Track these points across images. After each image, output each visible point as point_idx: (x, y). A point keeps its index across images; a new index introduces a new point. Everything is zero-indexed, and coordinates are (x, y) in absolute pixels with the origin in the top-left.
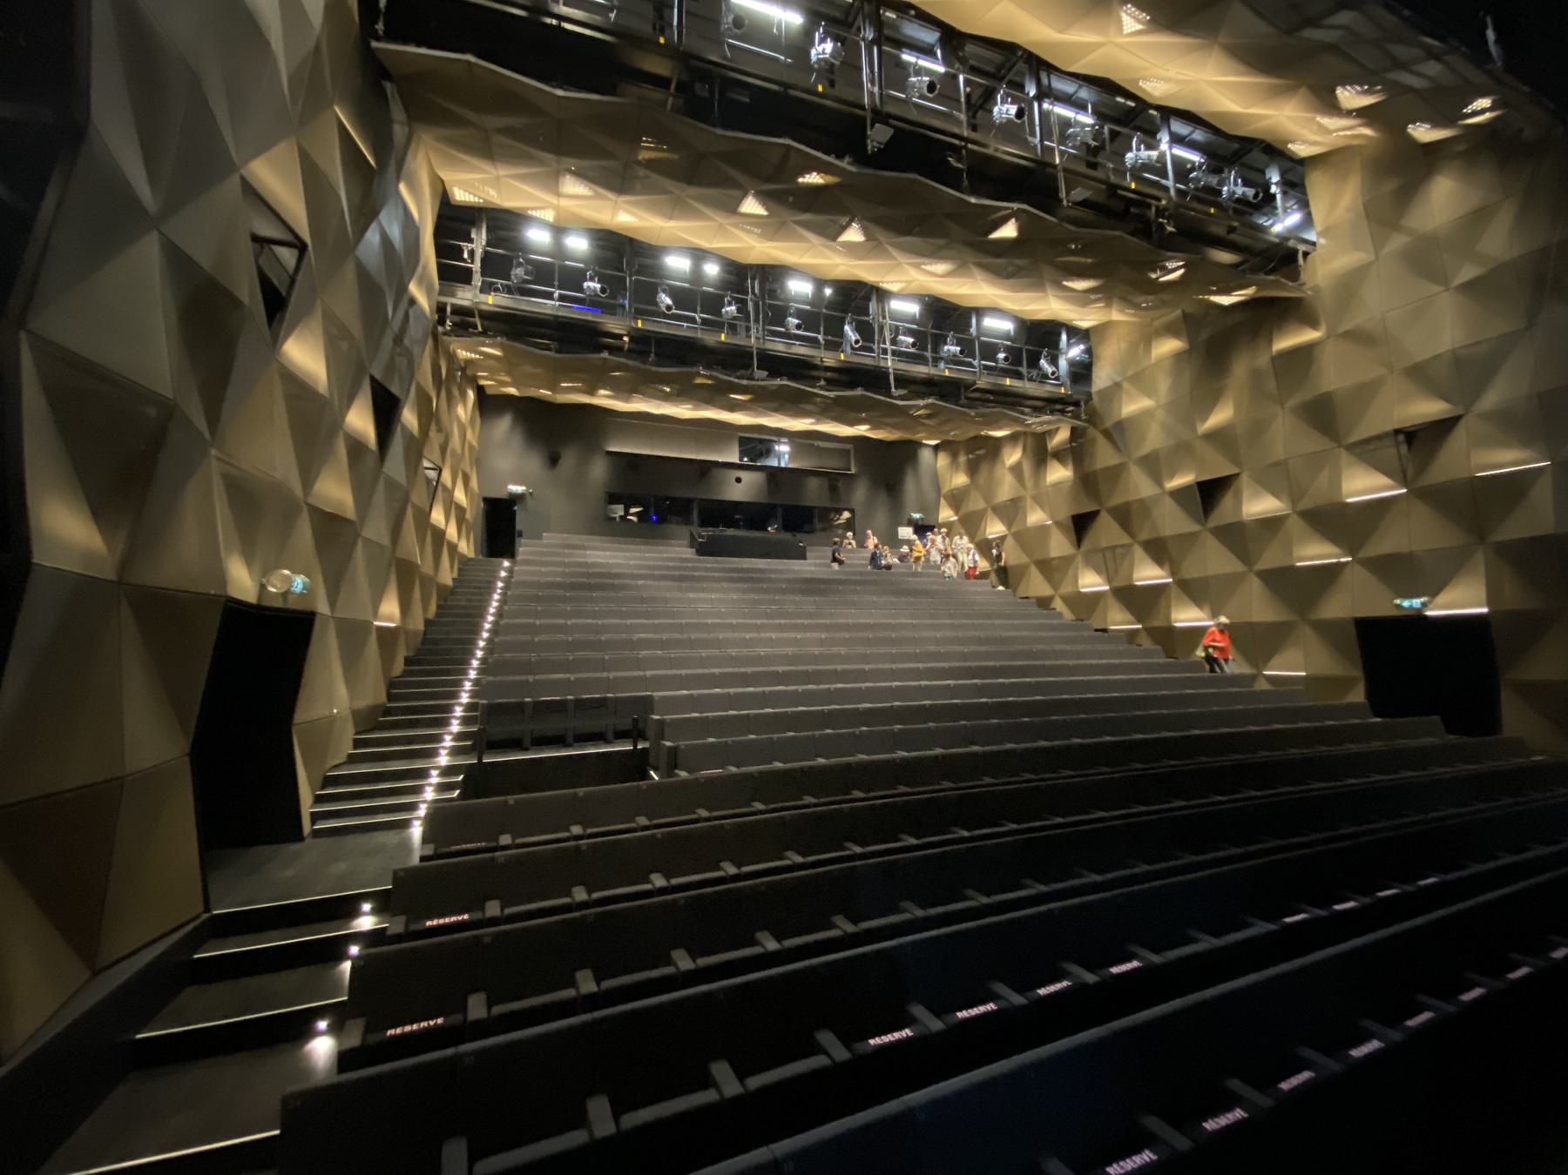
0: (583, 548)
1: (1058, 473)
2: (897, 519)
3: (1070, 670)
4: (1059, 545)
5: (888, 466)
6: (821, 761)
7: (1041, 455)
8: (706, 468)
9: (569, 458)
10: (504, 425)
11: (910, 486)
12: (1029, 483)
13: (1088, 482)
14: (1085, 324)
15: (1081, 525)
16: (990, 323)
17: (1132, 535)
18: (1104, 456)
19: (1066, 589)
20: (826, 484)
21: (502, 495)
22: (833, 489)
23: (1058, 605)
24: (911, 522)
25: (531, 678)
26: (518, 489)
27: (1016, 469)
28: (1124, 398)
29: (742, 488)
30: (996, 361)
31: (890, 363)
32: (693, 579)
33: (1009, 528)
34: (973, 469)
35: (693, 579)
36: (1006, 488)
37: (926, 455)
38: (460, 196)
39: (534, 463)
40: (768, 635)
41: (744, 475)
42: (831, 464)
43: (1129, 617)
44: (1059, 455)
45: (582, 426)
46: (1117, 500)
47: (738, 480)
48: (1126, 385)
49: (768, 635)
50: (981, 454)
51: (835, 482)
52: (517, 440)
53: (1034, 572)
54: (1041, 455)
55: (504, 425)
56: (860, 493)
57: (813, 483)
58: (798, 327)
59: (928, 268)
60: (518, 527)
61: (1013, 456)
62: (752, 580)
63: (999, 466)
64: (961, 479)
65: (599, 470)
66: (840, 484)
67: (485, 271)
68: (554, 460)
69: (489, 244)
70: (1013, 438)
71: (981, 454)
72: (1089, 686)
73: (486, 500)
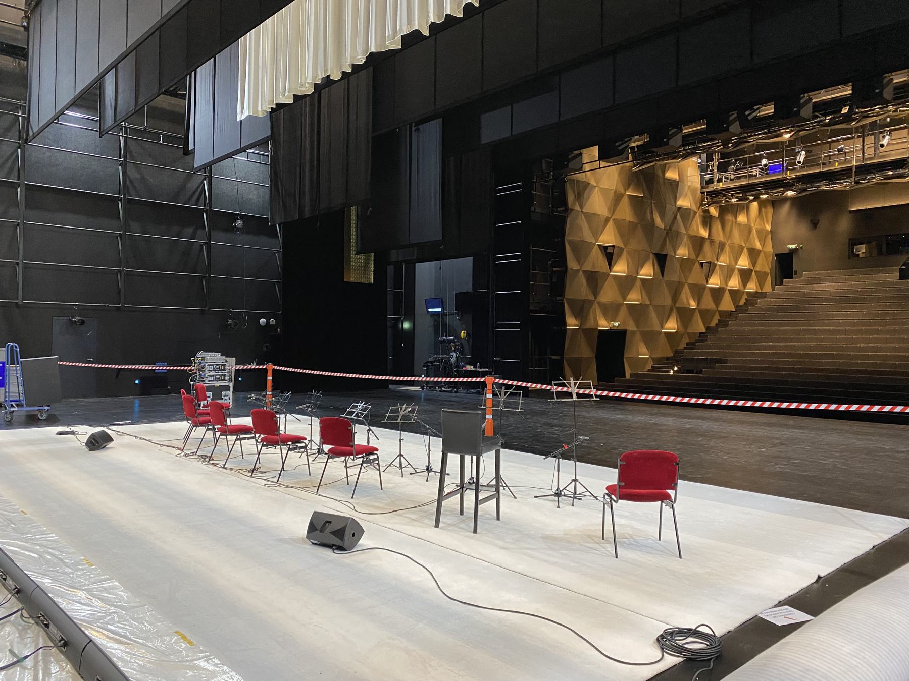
9: (824, 221)
21: (787, 251)
26: (794, 246)
52: (793, 218)
65: (844, 225)
68: (815, 225)
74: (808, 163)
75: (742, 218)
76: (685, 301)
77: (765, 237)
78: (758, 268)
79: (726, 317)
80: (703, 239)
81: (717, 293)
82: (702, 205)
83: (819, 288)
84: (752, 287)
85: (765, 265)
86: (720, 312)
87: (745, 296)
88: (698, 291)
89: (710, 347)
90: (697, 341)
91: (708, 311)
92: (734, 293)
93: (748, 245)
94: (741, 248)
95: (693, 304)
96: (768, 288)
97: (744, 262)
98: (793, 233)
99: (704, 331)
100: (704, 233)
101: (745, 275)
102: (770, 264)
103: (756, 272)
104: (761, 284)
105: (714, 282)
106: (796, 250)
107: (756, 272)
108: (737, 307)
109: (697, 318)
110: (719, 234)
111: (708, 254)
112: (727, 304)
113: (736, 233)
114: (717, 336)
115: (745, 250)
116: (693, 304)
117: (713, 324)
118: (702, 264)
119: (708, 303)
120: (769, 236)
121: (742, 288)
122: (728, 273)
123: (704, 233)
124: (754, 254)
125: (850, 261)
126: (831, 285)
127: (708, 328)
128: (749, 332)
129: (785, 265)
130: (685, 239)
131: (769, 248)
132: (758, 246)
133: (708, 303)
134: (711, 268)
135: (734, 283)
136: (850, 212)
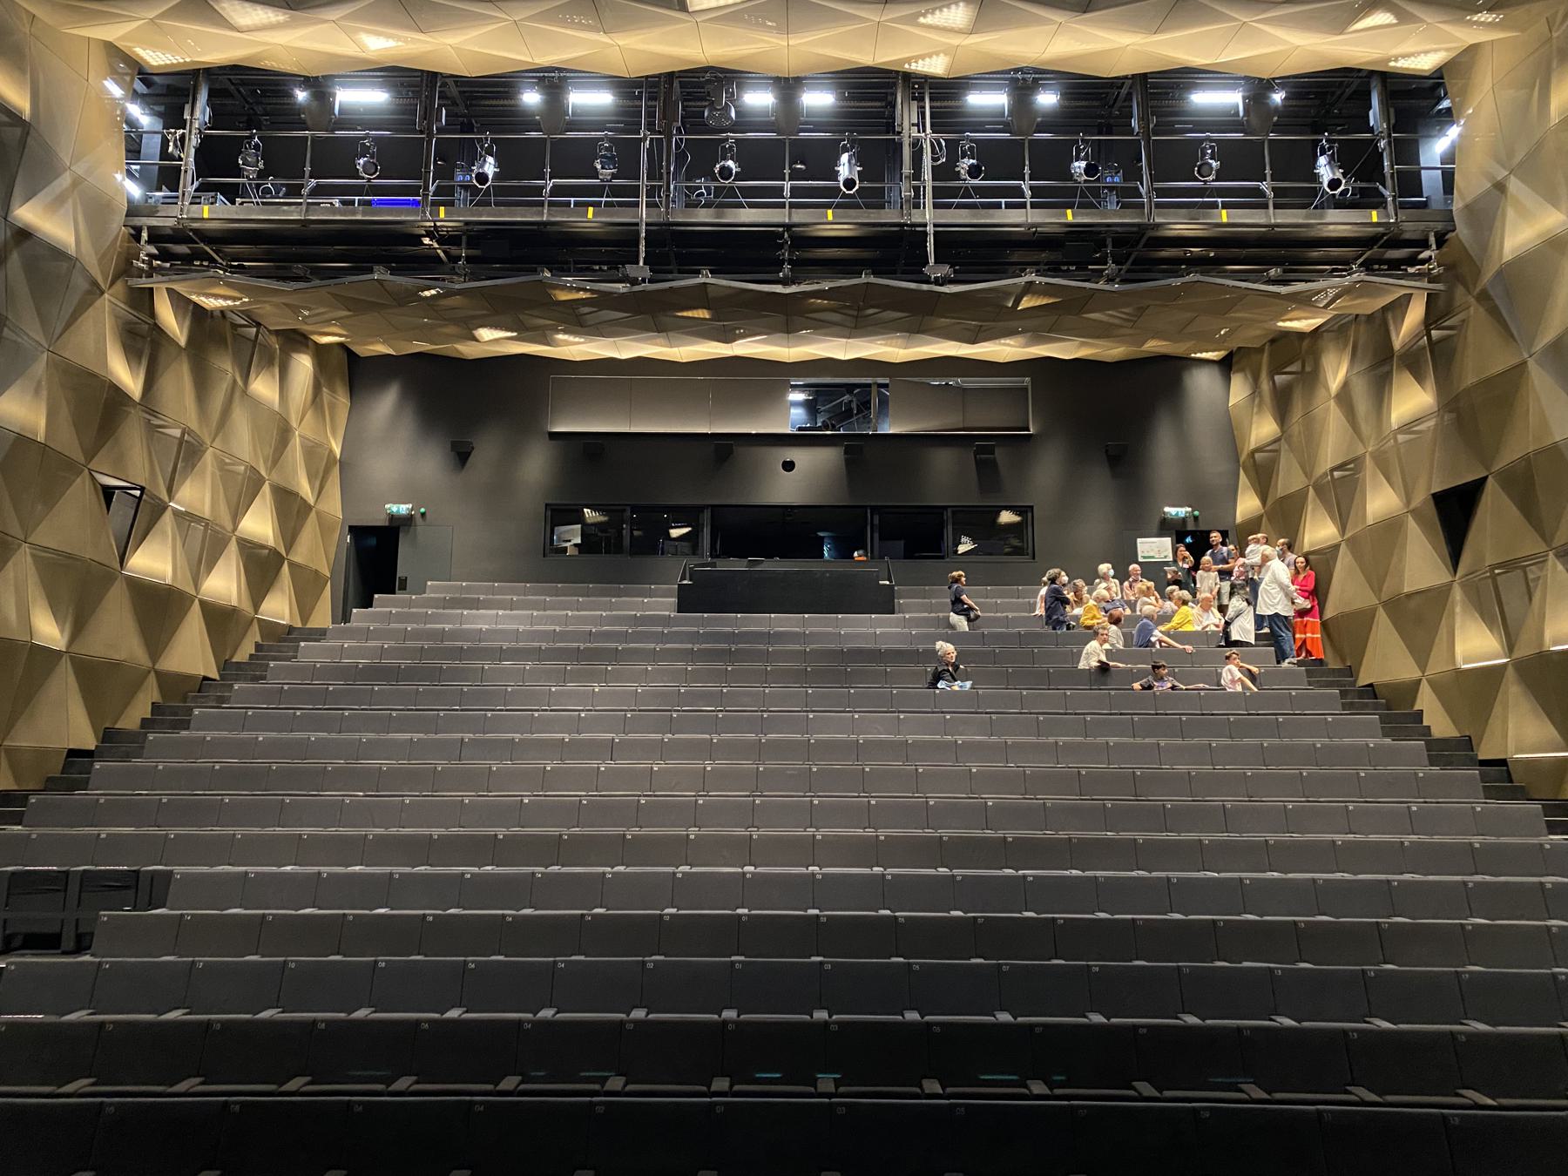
0: (475, 604)
1: (1412, 400)
2: (1136, 516)
3: (1199, 855)
4: (1421, 563)
5: (1114, 415)
6: (1192, 1020)
7: (1382, 364)
8: (725, 447)
9: (486, 450)
10: (386, 403)
11: (1164, 449)
12: (1365, 428)
13: (1474, 414)
14: (1425, 63)
15: (1454, 512)
16: (1204, 99)
17: (1546, 537)
18: (1483, 357)
19: (1436, 666)
20: (969, 456)
21: (381, 521)
22: (987, 470)
23: (1426, 701)
24: (1168, 527)
25: (693, 832)
26: (403, 509)
27: (1344, 397)
28: (1511, 213)
29: (800, 479)
30: (1070, 177)
31: (928, 216)
32: (615, 656)
33: (1343, 529)
34: (1282, 405)
35: (615, 656)
36: (1332, 446)
37: (1202, 383)
38: (156, 58)
39: (431, 465)
40: (538, 764)
41: (798, 455)
42: (987, 419)
43: (1550, 732)
44: (1413, 363)
45: (517, 388)
46: (1512, 452)
47: (788, 466)
48: (1514, 185)
49: (538, 764)
50: (1286, 365)
51: (989, 454)
52: (407, 427)
53: (1384, 632)
54: (1382, 364)
55: (386, 403)
56: (1045, 474)
57: (943, 461)
58: (974, 172)
59: (929, 20)
60: (401, 572)
61: (1337, 371)
62: (728, 656)
63: (1321, 393)
64: (1263, 429)
65: (536, 468)
66: (1000, 454)
67: (201, 171)
68: (462, 456)
69: (216, 122)
70: (1338, 330)
71: (1286, 365)
72: (1241, 894)
73: (357, 532)
74: (503, 194)
75: (263, 387)
76: (12, 615)
77: (327, 471)
78: (299, 555)
79: (181, 699)
80: (117, 395)
81: (158, 608)
82: (126, 269)
83: (482, 621)
84: (278, 607)
85: (320, 550)
86: (160, 675)
87: (252, 639)
88: (80, 586)
89: (92, 814)
90: (51, 784)
91: (115, 666)
92: (220, 620)
93: (276, 477)
94: (254, 485)
95: (49, 631)
96: (322, 616)
97: (259, 524)
98: (397, 468)
99: (89, 742)
100: (129, 379)
101: (262, 568)
102: (333, 550)
103: (292, 565)
104: (304, 605)
105: (153, 561)
106: (408, 520)
107: (292, 565)
108: (226, 666)
109: (64, 690)
110: (179, 399)
111: (134, 463)
112: (191, 652)
113: (241, 423)
114: (137, 762)
115: (266, 488)
116: (49, 631)
117: (130, 720)
118: (108, 492)
119: (116, 635)
120: (336, 470)
121: (247, 606)
122: (207, 544)
123: (129, 379)
124: (290, 510)
125: (543, 565)
126: (509, 616)
127: (109, 736)
128: (273, 749)
129: (375, 559)
130: (40, 367)
131: (333, 505)
132: (305, 490)
133: (116, 635)
134: (141, 513)
135: (224, 583)
136: (555, 436)
